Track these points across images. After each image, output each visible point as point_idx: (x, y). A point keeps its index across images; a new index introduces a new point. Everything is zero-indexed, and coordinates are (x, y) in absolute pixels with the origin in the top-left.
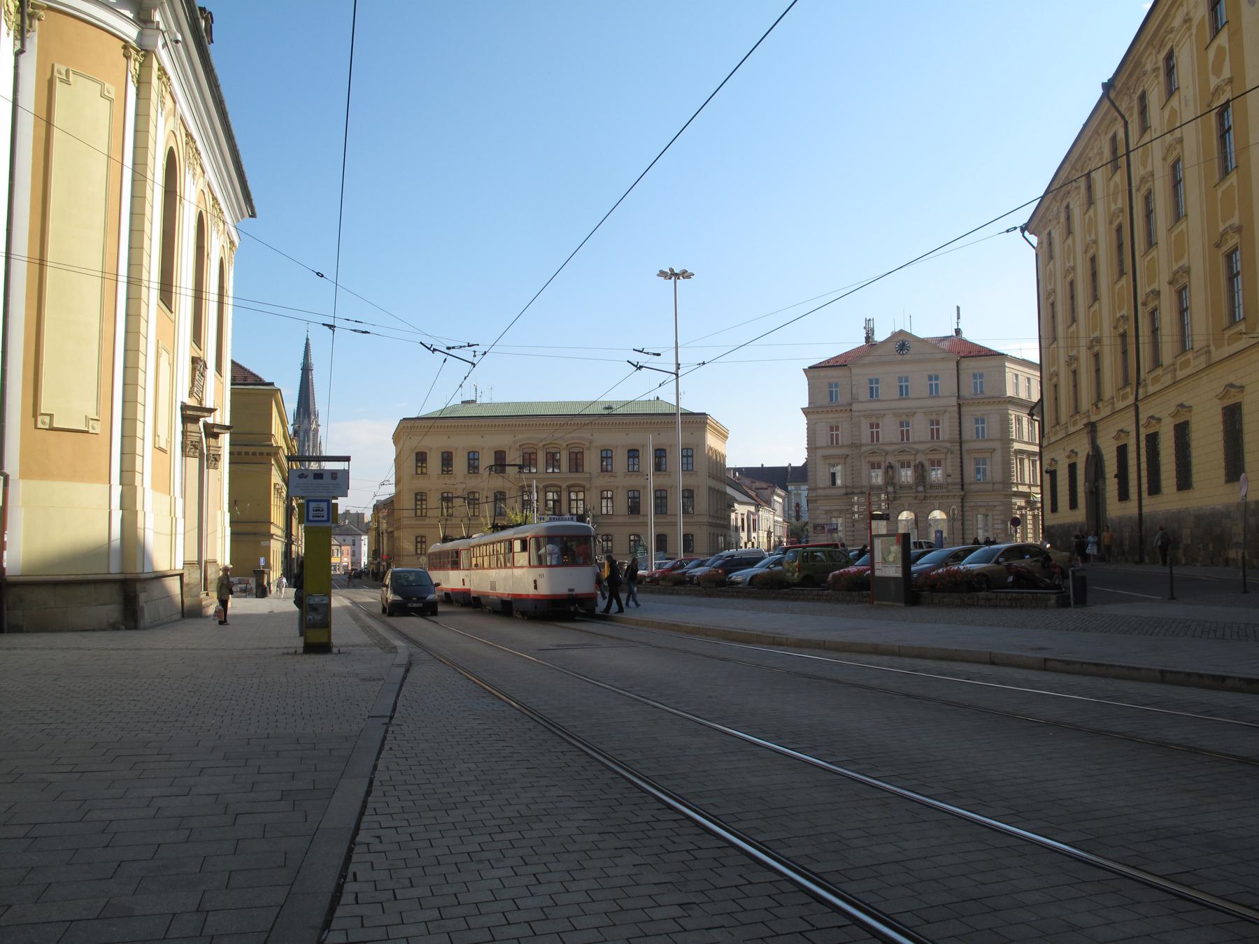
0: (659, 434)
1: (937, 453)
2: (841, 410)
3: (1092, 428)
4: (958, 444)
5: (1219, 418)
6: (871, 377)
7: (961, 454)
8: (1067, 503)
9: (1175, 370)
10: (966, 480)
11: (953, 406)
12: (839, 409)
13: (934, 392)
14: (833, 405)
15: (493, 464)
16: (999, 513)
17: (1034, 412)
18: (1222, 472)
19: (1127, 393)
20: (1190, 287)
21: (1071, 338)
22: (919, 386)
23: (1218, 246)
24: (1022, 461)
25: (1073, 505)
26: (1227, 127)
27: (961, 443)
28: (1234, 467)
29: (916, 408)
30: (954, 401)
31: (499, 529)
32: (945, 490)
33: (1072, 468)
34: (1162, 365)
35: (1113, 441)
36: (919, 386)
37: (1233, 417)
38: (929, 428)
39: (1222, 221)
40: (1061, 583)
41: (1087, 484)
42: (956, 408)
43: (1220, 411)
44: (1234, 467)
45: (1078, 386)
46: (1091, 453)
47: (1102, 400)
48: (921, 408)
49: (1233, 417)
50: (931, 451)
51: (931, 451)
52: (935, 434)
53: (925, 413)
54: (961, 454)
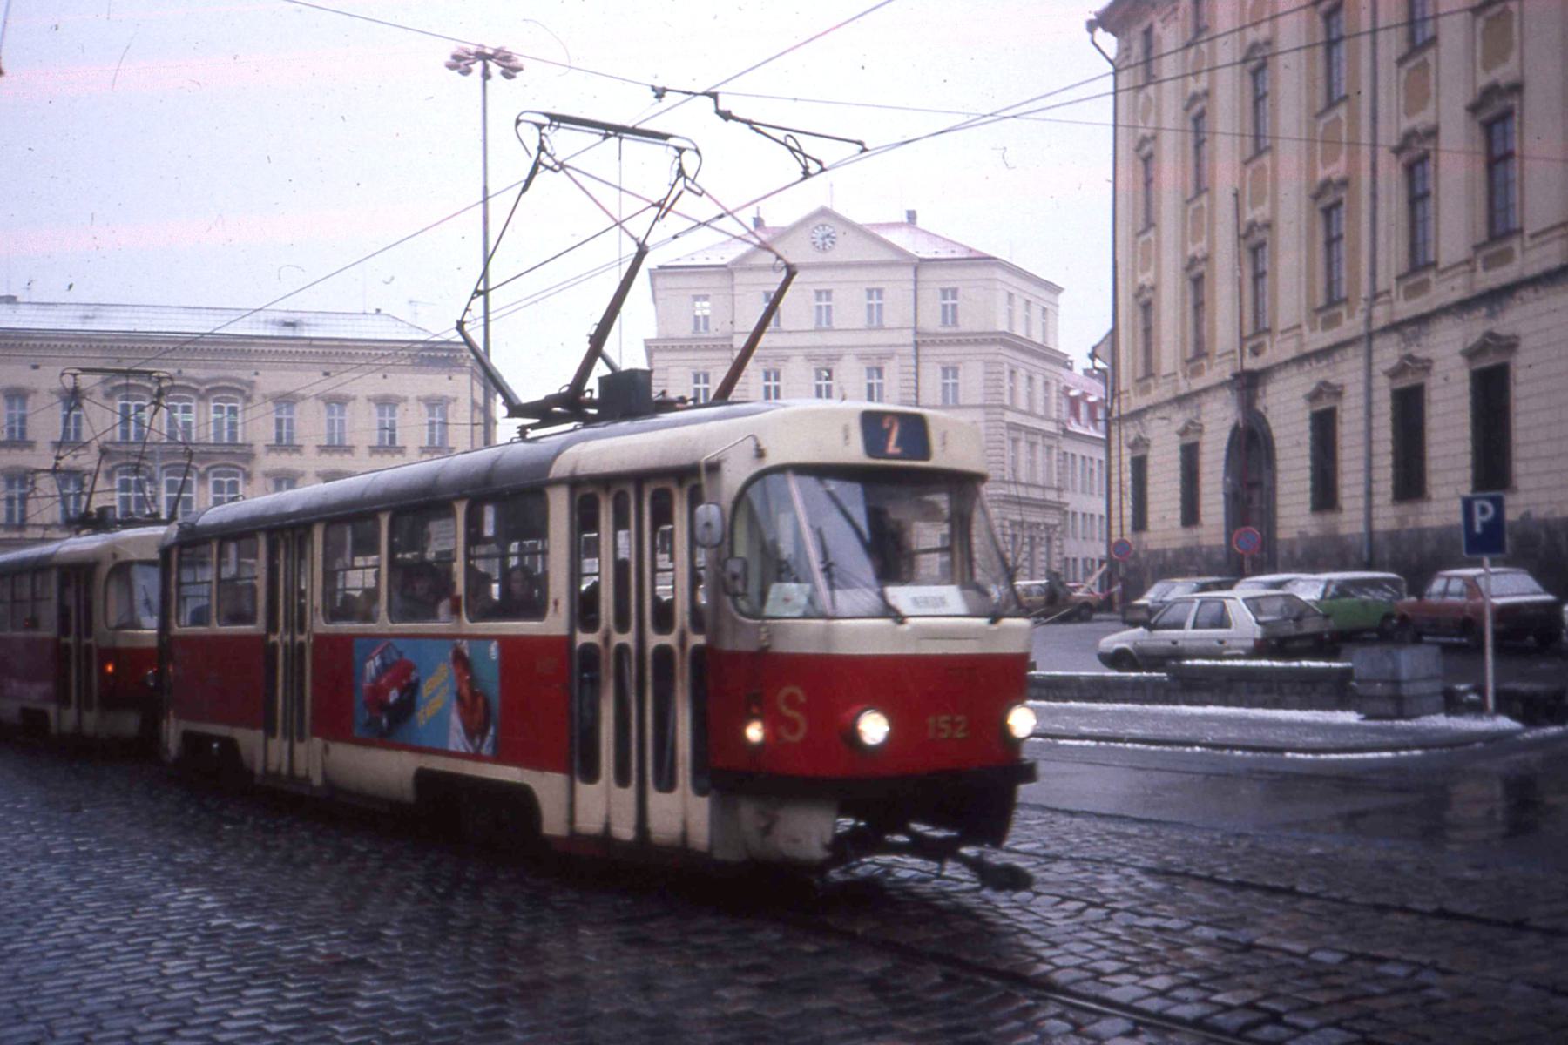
0: (385, 377)
2: (698, 346)
3: (1248, 384)
5: (1178, 454)
6: (767, 289)
9: (1473, 270)
11: (904, 345)
12: (702, 343)
17: (1099, 352)
18: (1178, 515)
19: (1340, 314)
20: (1521, 116)
21: (1315, 141)
23: (1245, 237)
24: (1033, 445)
25: (1191, 515)
26: (1261, 92)
30: (908, 337)
33: (1190, 457)
34: (1435, 264)
35: (1177, 438)
39: (1322, 161)
41: (1228, 480)
42: (911, 350)
43: (1307, 414)
45: (1154, 333)
46: (1241, 425)
47: (1206, 355)
48: (852, 347)
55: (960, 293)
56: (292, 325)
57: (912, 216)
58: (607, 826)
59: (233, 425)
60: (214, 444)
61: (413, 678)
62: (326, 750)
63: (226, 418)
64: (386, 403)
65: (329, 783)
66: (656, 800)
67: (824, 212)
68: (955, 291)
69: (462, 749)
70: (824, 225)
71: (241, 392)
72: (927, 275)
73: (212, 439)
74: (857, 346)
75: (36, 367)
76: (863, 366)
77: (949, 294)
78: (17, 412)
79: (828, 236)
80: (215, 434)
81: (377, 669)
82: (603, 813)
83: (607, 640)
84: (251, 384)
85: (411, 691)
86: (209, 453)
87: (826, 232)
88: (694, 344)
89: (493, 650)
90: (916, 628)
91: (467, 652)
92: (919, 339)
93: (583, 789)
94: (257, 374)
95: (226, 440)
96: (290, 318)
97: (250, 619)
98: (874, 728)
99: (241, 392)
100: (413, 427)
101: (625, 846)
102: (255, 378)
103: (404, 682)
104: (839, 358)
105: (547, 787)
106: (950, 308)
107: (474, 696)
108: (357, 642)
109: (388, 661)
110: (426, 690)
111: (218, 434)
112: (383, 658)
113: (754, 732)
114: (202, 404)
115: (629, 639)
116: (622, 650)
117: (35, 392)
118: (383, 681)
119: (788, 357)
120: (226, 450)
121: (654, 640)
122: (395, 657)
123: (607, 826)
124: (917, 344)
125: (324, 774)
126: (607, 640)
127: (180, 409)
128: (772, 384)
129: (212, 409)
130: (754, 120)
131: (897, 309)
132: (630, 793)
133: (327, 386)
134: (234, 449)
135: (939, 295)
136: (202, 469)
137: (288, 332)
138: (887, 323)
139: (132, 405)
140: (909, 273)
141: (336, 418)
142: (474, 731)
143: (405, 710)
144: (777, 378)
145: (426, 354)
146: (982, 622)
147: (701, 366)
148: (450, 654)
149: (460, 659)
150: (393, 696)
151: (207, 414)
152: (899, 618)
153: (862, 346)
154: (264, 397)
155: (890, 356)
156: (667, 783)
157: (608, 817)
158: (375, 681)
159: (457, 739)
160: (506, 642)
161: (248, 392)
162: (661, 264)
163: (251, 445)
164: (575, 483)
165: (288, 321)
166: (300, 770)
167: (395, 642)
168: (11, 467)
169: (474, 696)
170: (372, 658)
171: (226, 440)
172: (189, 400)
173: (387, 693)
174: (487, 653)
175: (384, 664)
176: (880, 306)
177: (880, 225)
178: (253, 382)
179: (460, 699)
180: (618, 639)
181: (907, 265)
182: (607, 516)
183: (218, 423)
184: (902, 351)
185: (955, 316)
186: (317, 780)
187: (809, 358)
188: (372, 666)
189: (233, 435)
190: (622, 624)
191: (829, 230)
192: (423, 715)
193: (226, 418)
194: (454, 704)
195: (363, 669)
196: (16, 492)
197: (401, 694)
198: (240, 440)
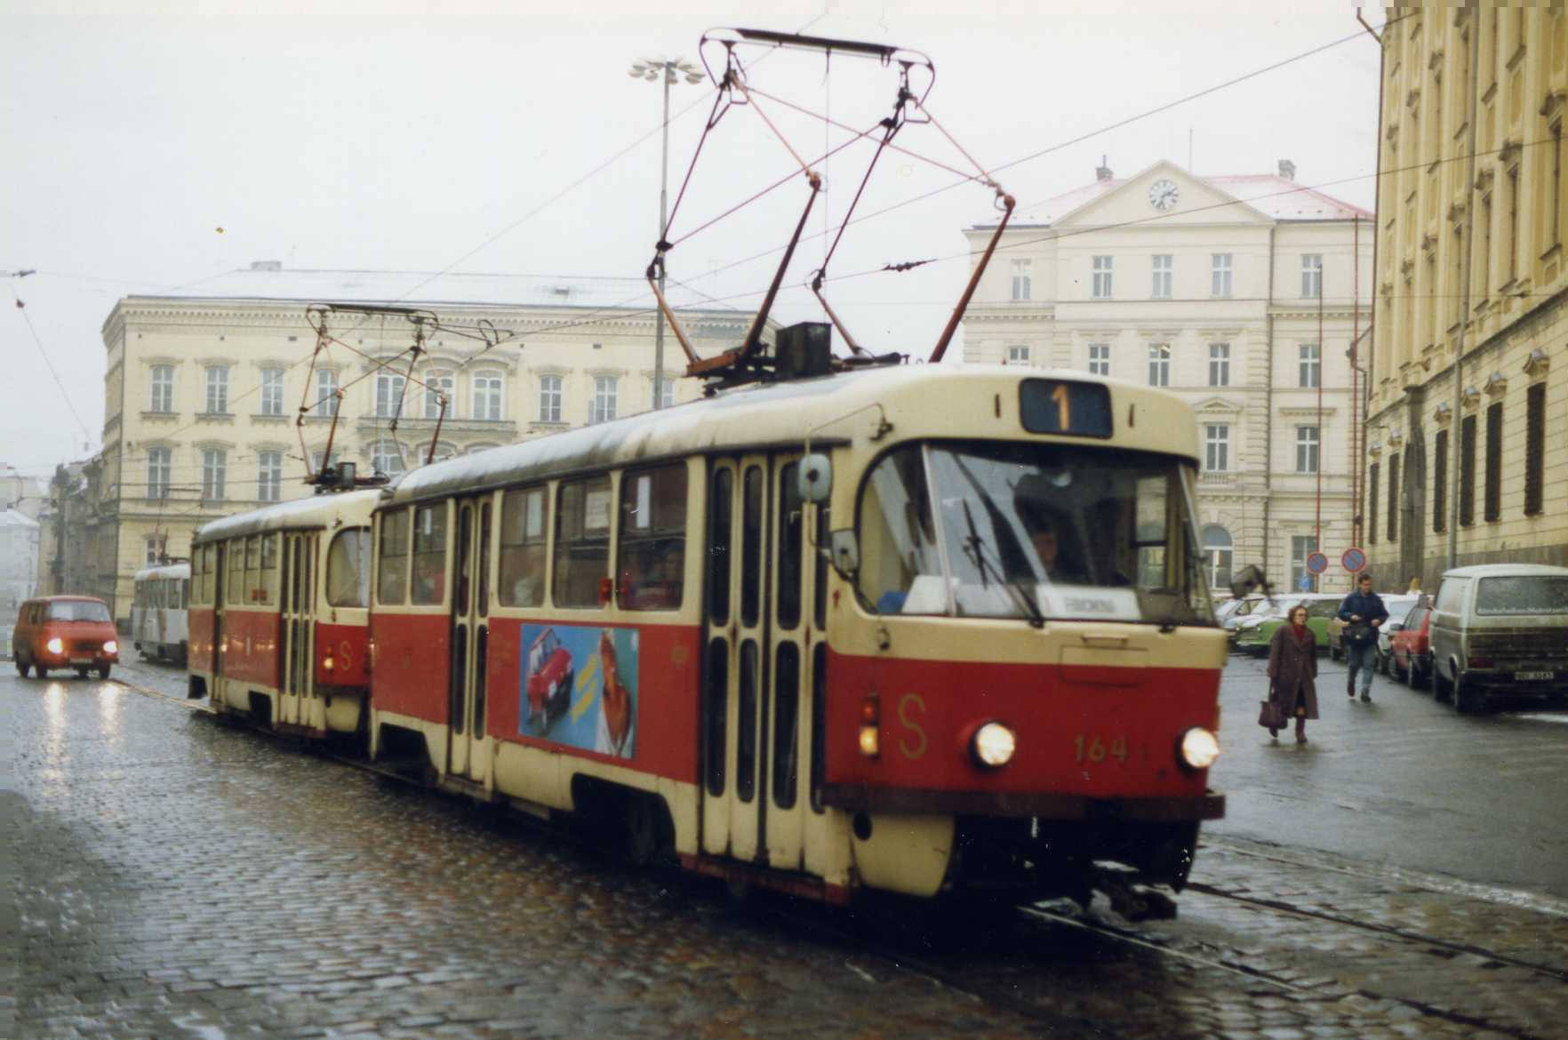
1: (1220, 412)
2: (1016, 317)
4: (1264, 395)
7: (1269, 416)
8: (1521, 498)
10: (1275, 469)
11: (1257, 319)
13: (1221, 291)
14: (1019, 305)
15: (1326, 302)
16: (1337, 534)
22: (1192, 276)
27: (1270, 392)
28: (1533, 505)
29: (1122, 321)
30: (1260, 310)
31: (170, 561)
32: (1232, 486)
36: (1192, 276)
37: (1537, 396)
38: (1207, 360)
40: (640, 948)
42: (1263, 325)
44: (1533, 505)
49: (1537, 396)
50: (1210, 406)
51: (1210, 406)
52: (1218, 375)
53: (1204, 332)
54: (1269, 416)
55: (1115, 261)
56: (565, 292)
57: (1287, 168)
58: (729, 845)
59: (495, 399)
60: (489, 421)
61: (569, 670)
62: (496, 750)
63: (487, 391)
64: (216, 368)
65: (497, 792)
66: (774, 812)
67: (1163, 166)
68: (1168, 258)
69: (606, 751)
70: (1165, 182)
71: (505, 365)
72: (1284, 237)
73: (472, 416)
74: (1199, 320)
75: (293, 339)
76: (1206, 343)
77: (1163, 261)
78: (217, 383)
79: (1169, 194)
80: (476, 410)
81: (539, 659)
82: (725, 832)
83: (734, 633)
84: (516, 358)
85: (567, 682)
86: (469, 430)
87: (1166, 189)
88: (1012, 314)
89: (635, 639)
90: (1055, 635)
91: (613, 642)
92: (1275, 312)
93: (710, 801)
94: (522, 346)
95: (487, 416)
96: (562, 285)
97: (437, 600)
98: (996, 744)
99: (505, 365)
100: (577, 397)
101: (292, 725)
102: (521, 351)
103: (562, 674)
104: (1176, 332)
105: (680, 797)
106: (1162, 276)
107: (618, 689)
108: (523, 626)
109: (548, 650)
110: (579, 683)
111: (478, 410)
112: (544, 647)
113: (868, 740)
114: (463, 377)
115: (755, 634)
116: (748, 644)
117: (181, 362)
118: (544, 673)
119: (1120, 330)
120: (486, 427)
121: (779, 635)
122: (555, 646)
123: (729, 845)
124: (1271, 319)
125: (495, 783)
126: (734, 633)
127: (488, 384)
128: (1220, 360)
129: (473, 384)
130: (707, 121)
131: (1249, 277)
132: (754, 805)
133: (598, 360)
134: (493, 426)
135: (1300, 261)
136: (412, 445)
137: (559, 300)
138: (1236, 292)
139: (391, 378)
140: (1264, 236)
141: (163, 382)
142: (617, 732)
143: (560, 705)
144: (1105, 355)
145: (707, 324)
146: (1153, 629)
147: (1018, 341)
148: (599, 644)
149: (608, 650)
150: (552, 689)
151: (468, 389)
152: (1037, 620)
153: (1206, 320)
154: (530, 371)
155: (1237, 332)
156: (786, 798)
157: (729, 835)
158: (537, 673)
159: (603, 744)
160: (647, 631)
161: (512, 365)
162: (977, 223)
163: (514, 423)
164: (712, 455)
165: (560, 288)
166: (476, 774)
167: (558, 630)
168: (266, 443)
169: (618, 689)
170: (535, 647)
171: (487, 416)
172: (495, 374)
173: (546, 685)
174: (629, 642)
175: (545, 654)
176: (1228, 274)
177: (1237, 179)
178: (519, 355)
179: (606, 693)
180: (745, 633)
181: (1259, 227)
182: (738, 497)
183: (479, 398)
184: (1253, 326)
185: (1027, 289)
186: (488, 785)
187: (1144, 332)
188: (535, 655)
189: (495, 412)
190: (750, 616)
191: (1169, 188)
192: (577, 710)
193: (487, 391)
194: (601, 699)
195: (527, 657)
196: (269, 468)
197: (559, 687)
198: (502, 418)
